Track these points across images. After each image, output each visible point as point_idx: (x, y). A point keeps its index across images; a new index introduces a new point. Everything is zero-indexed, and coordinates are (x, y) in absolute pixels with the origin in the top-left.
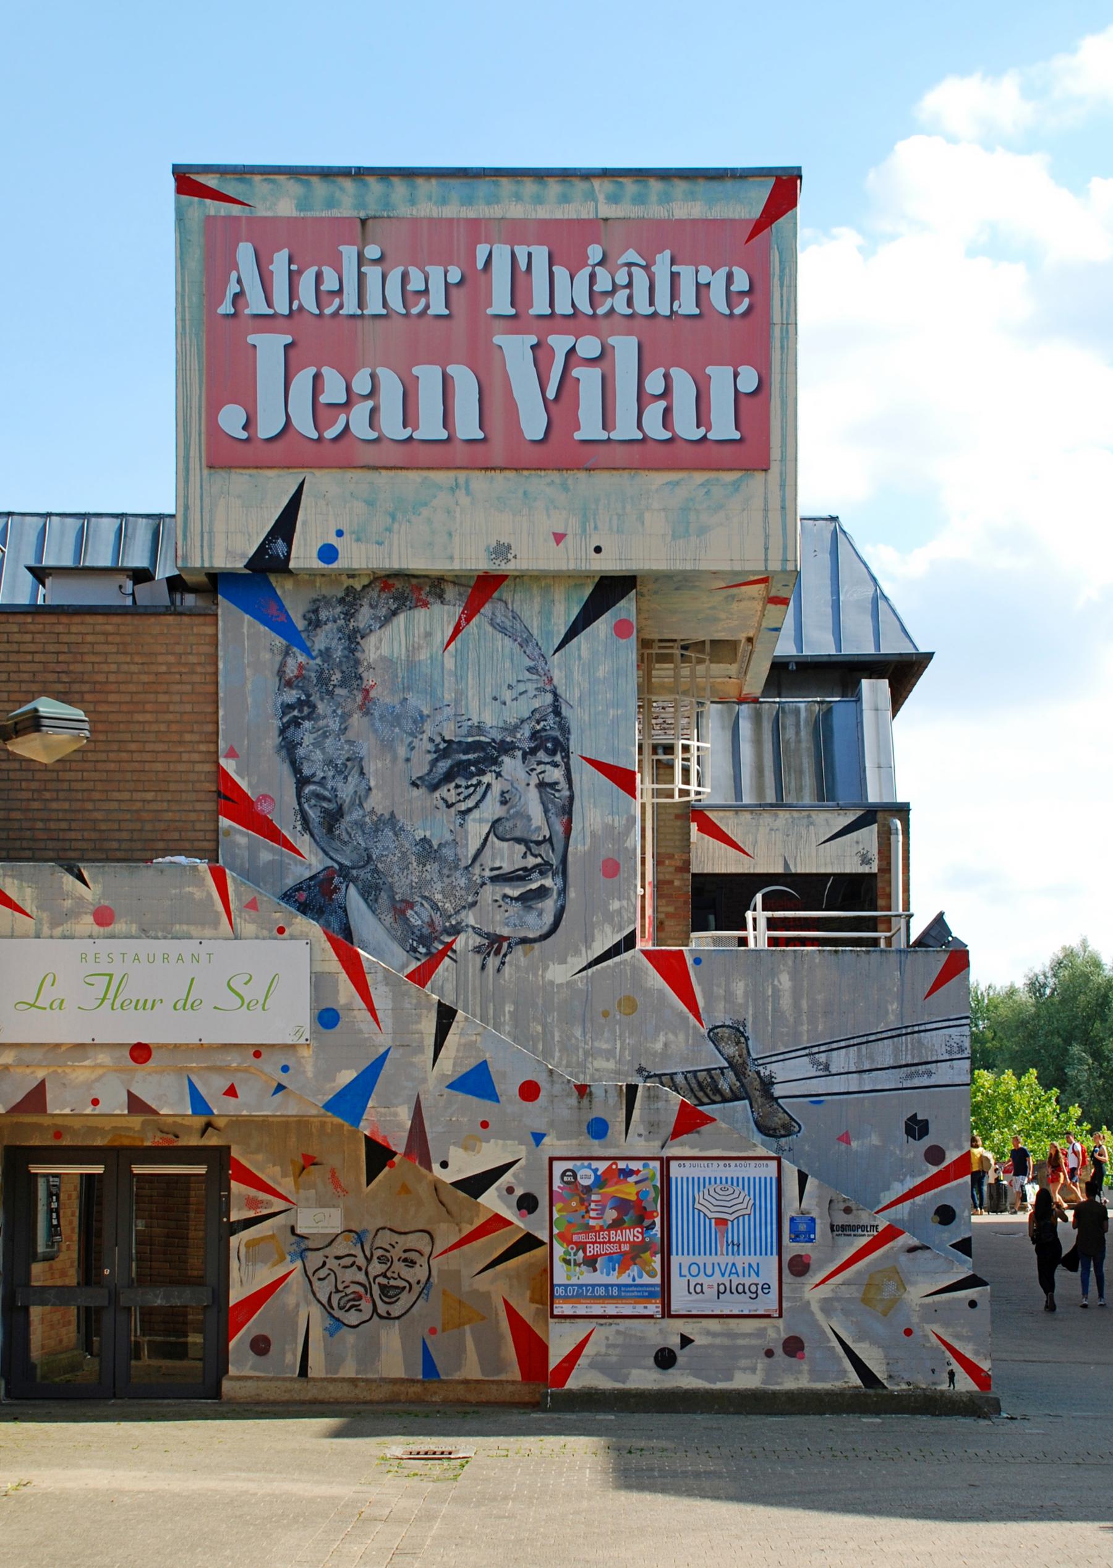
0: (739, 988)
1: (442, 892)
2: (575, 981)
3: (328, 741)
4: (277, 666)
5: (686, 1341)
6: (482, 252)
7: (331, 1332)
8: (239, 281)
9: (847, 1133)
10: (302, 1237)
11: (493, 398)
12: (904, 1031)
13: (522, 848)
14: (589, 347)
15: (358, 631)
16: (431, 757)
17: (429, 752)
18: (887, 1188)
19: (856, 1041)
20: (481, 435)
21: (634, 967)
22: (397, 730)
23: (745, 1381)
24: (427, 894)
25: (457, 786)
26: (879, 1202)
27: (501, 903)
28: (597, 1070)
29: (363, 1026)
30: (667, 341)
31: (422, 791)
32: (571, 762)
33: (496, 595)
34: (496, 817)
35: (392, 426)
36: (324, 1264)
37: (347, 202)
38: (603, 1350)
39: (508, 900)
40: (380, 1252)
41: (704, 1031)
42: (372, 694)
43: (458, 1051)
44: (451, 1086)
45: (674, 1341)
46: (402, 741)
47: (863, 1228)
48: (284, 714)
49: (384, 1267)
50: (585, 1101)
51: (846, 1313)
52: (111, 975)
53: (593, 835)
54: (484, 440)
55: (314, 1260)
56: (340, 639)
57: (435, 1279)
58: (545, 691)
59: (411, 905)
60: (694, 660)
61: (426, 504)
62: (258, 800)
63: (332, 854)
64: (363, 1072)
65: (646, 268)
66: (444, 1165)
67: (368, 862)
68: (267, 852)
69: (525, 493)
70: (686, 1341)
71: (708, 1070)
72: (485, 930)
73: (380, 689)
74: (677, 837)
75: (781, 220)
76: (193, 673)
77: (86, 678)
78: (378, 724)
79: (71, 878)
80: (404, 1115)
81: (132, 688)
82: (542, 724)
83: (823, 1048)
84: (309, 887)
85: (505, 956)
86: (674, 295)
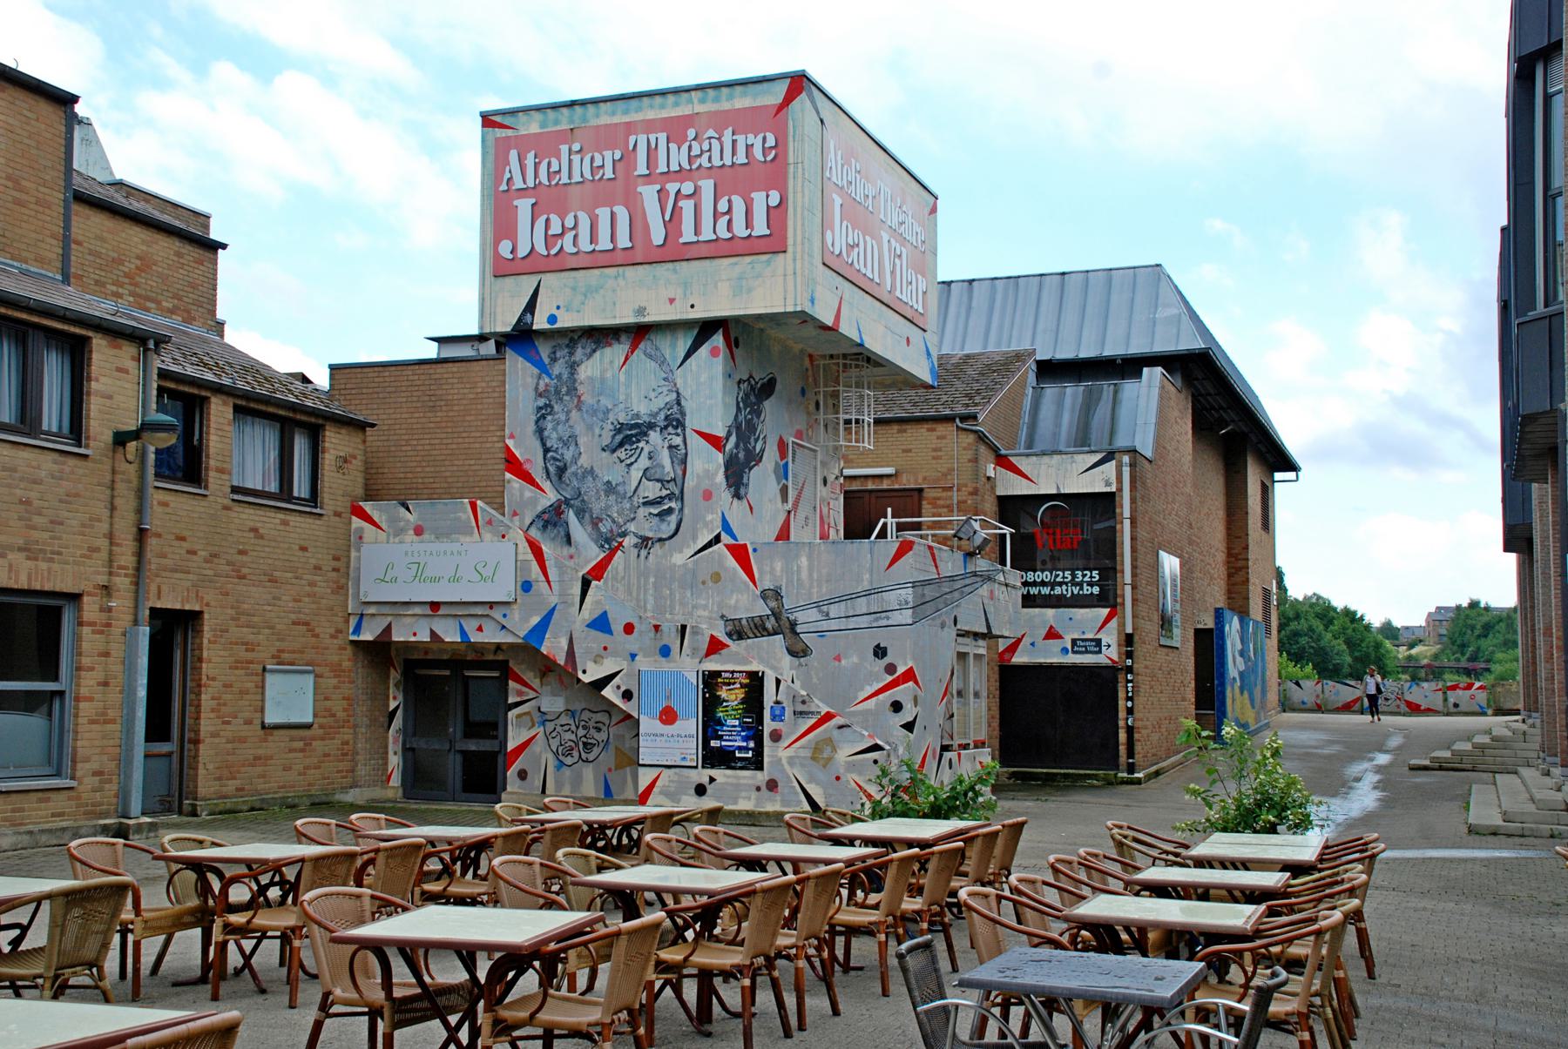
0: (778, 566)
5: (712, 780)
6: (632, 139)
7: (558, 768)
11: (638, 224)
14: (688, 188)
18: (862, 689)
21: (720, 555)
23: (744, 805)
30: (731, 180)
35: (585, 245)
37: (564, 121)
45: (706, 780)
51: (802, 765)
55: (550, 726)
65: (719, 139)
70: (712, 780)
80: (564, 644)
86: (734, 153)
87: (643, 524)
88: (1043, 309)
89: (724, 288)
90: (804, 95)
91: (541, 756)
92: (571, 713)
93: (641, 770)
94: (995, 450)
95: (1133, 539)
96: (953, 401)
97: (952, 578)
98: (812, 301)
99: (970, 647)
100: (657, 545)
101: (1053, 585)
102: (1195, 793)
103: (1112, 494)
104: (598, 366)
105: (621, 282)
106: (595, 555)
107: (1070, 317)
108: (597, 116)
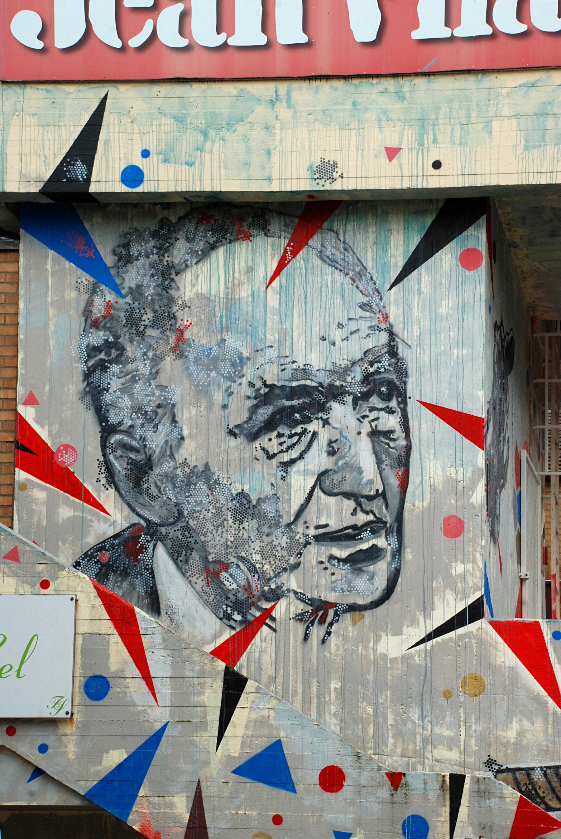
1: (261, 552)
2: (411, 656)
3: (137, 386)
4: (83, 305)
13: (351, 504)
15: (173, 267)
16: (250, 403)
17: (249, 398)
20: (304, 39)
21: (481, 642)
22: (213, 374)
24: (243, 554)
25: (280, 435)
27: (328, 565)
28: (438, 761)
29: (138, 700)
32: (409, 408)
33: (325, 225)
34: (322, 469)
35: (205, 33)
39: (335, 562)
42: (187, 335)
43: (247, 728)
44: (238, 771)
46: (219, 385)
50: (400, 793)
54: (308, 45)
56: (153, 275)
58: (380, 330)
59: (226, 567)
62: (59, 450)
63: (138, 510)
64: (134, 753)
67: (178, 519)
68: (68, 508)
69: (354, 104)
73: (195, 330)
78: (192, 367)
80: (182, 807)
82: (376, 365)
84: (113, 546)
85: (331, 625)
87: (318, 576)
89: (506, 132)
104: (220, 279)
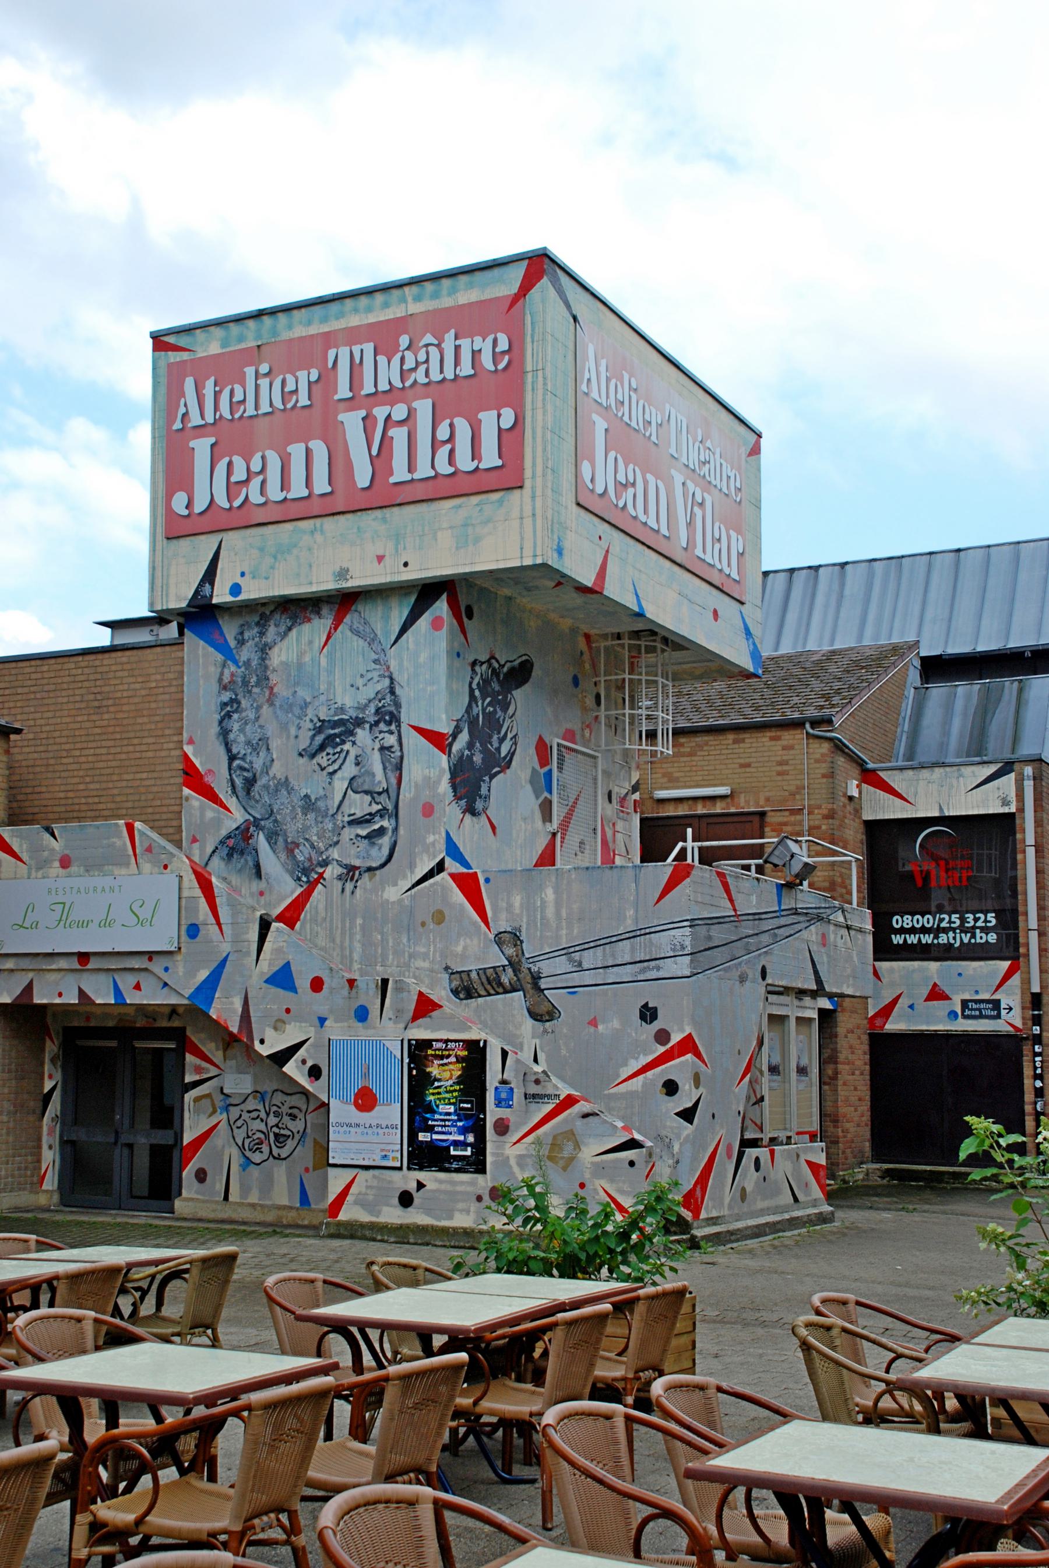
0: (517, 900)
1: (317, 834)
2: (403, 900)
4: (218, 676)
5: (420, 1186)
6: (331, 354)
7: (244, 1167)
8: (185, 405)
9: (595, 1018)
10: (228, 1096)
11: (339, 462)
12: (638, 933)
13: (368, 798)
14: (399, 412)
16: (311, 733)
18: (625, 1064)
19: (602, 942)
22: (290, 715)
23: (462, 1220)
25: (328, 754)
26: (618, 1076)
29: (215, 939)
30: (454, 398)
31: (306, 759)
33: (353, 608)
36: (241, 1116)
37: (250, 336)
38: (364, 1190)
40: (274, 1108)
41: (492, 936)
42: (275, 690)
43: (272, 954)
44: (266, 981)
45: (412, 1186)
47: (549, 1096)
48: (222, 709)
49: (278, 1119)
52: (64, 903)
53: (416, 785)
54: (331, 493)
55: (235, 1112)
57: (308, 1130)
58: (385, 677)
60: (659, 650)
61: (295, 546)
65: (438, 346)
66: (262, 1042)
67: (271, 815)
68: (212, 811)
70: (420, 1186)
71: (494, 968)
72: (345, 862)
74: (824, 791)
75: (532, 291)
76: (170, 686)
77: (111, 695)
78: (278, 712)
79: (48, 835)
81: (136, 700)
83: (577, 948)
86: (457, 362)
87: (350, 850)
88: (932, 595)
89: (445, 539)
90: (545, 280)
91: (224, 1150)
92: (259, 1094)
93: (330, 1170)
94: (860, 763)
95: (1039, 872)
96: (791, 701)
97: (757, 916)
98: (560, 552)
99: (790, 1008)
100: (366, 876)
101: (938, 931)
102: (995, 1238)
103: (1011, 816)
104: (296, 647)
105: (319, 538)
106: (289, 890)
107: (966, 603)
108: (290, 327)
